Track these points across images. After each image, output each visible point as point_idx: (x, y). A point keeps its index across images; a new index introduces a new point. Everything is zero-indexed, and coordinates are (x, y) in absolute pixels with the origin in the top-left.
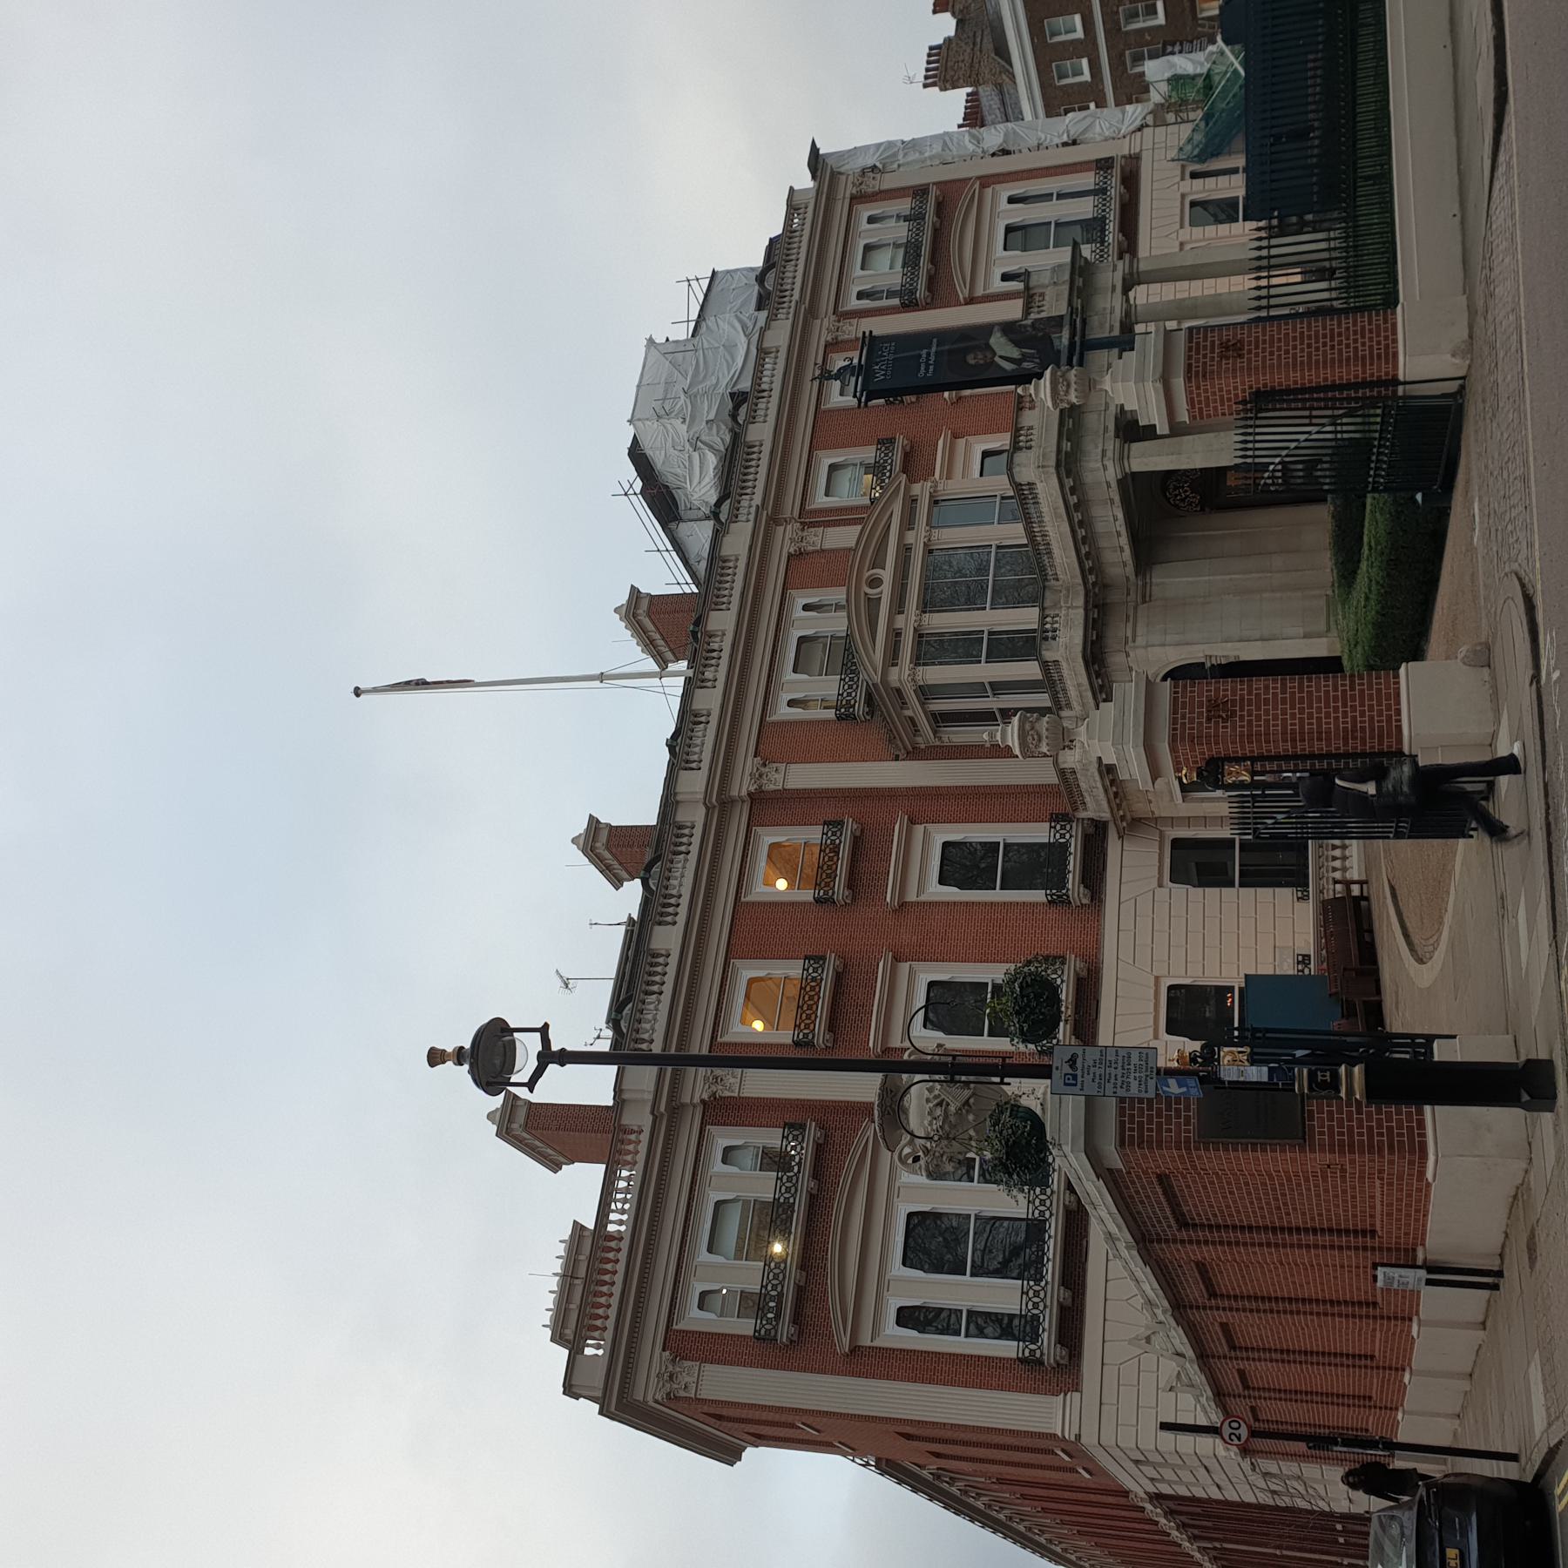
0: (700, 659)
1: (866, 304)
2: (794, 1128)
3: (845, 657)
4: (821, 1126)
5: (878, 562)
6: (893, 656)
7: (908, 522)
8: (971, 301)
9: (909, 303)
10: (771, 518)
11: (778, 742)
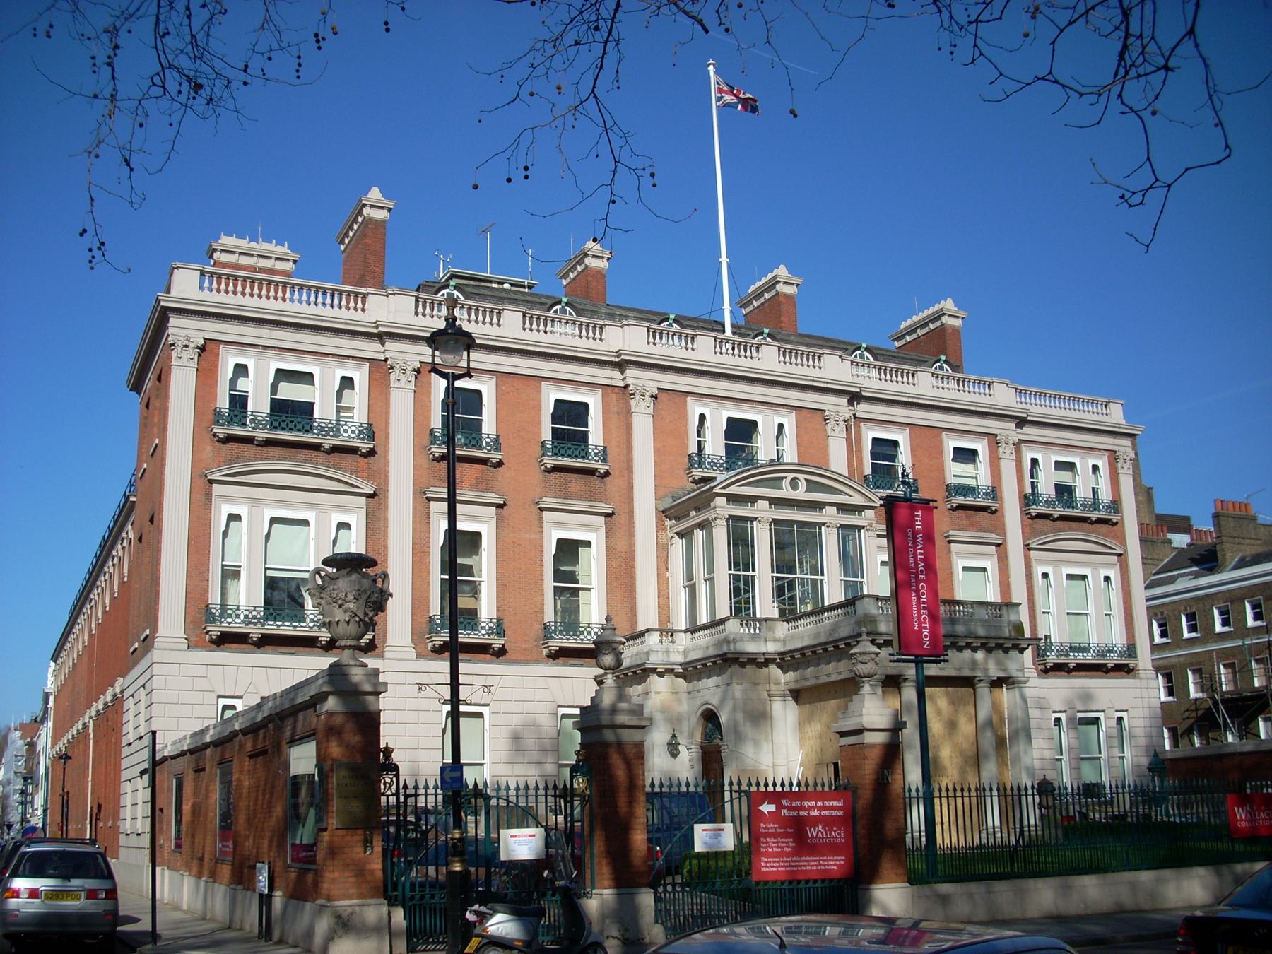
2: (369, 432)
4: (372, 453)
6: (732, 498)
7: (842, 508)
8: (1028, 548)
10: (855, 398)
11: (668, 403)
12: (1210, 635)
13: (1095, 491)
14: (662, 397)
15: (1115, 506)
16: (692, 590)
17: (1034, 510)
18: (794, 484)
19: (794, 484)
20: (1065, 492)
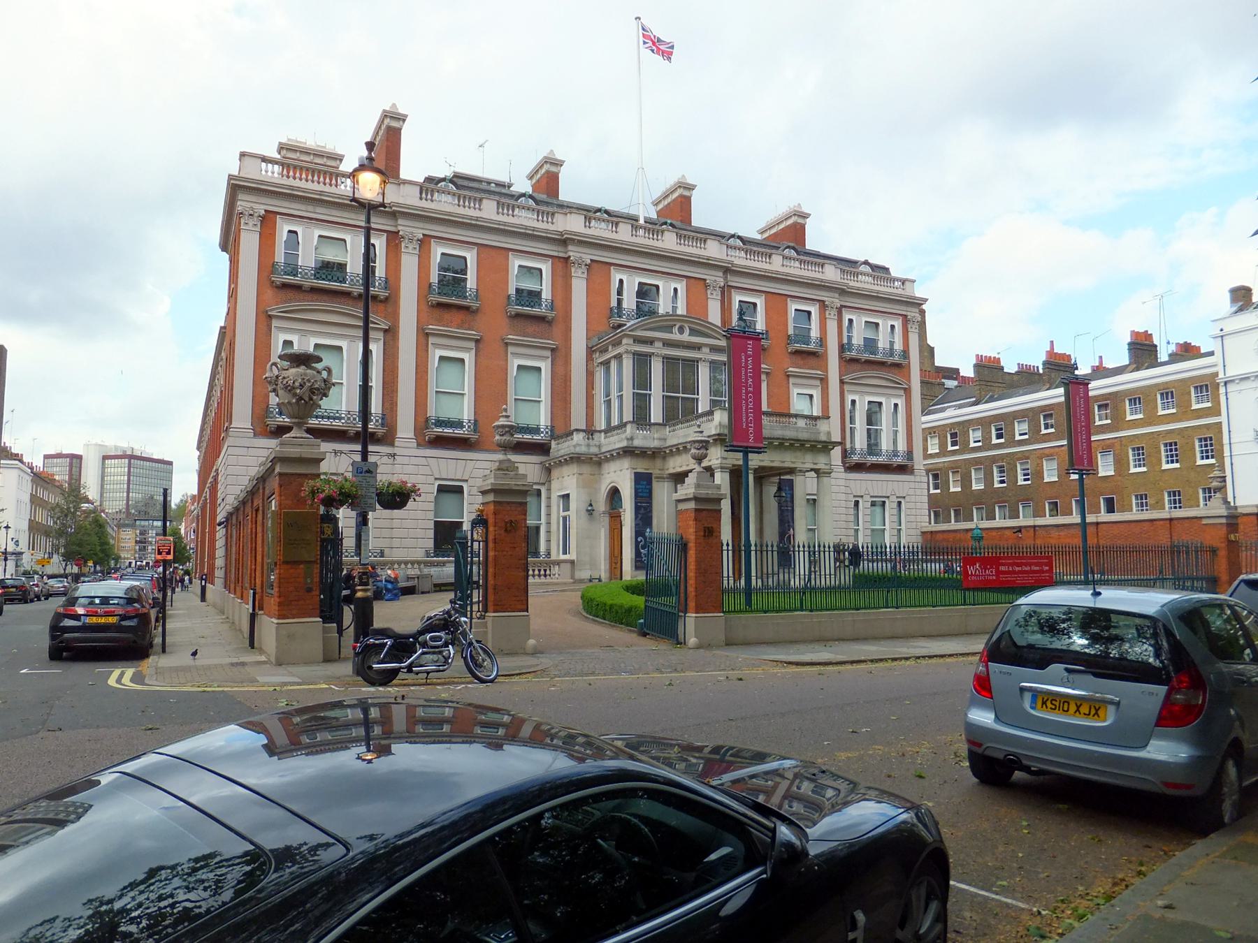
0: (653, 227)
1: (846, 323)
3: (645, 309)
4: (387, 299)
5: (693, 332)
6: (639, 340)
8: (842, 382)
9: (842, 348)
10: (727, 270)
11: (599, 271)
12: (966, 448)
13: (892, 343)
14: (595, 265)
15: (905, 353)
16: (608, 403)
17: (848, 354)
18: (681, 330)
19: (681, 330)
20: (870, 344)
